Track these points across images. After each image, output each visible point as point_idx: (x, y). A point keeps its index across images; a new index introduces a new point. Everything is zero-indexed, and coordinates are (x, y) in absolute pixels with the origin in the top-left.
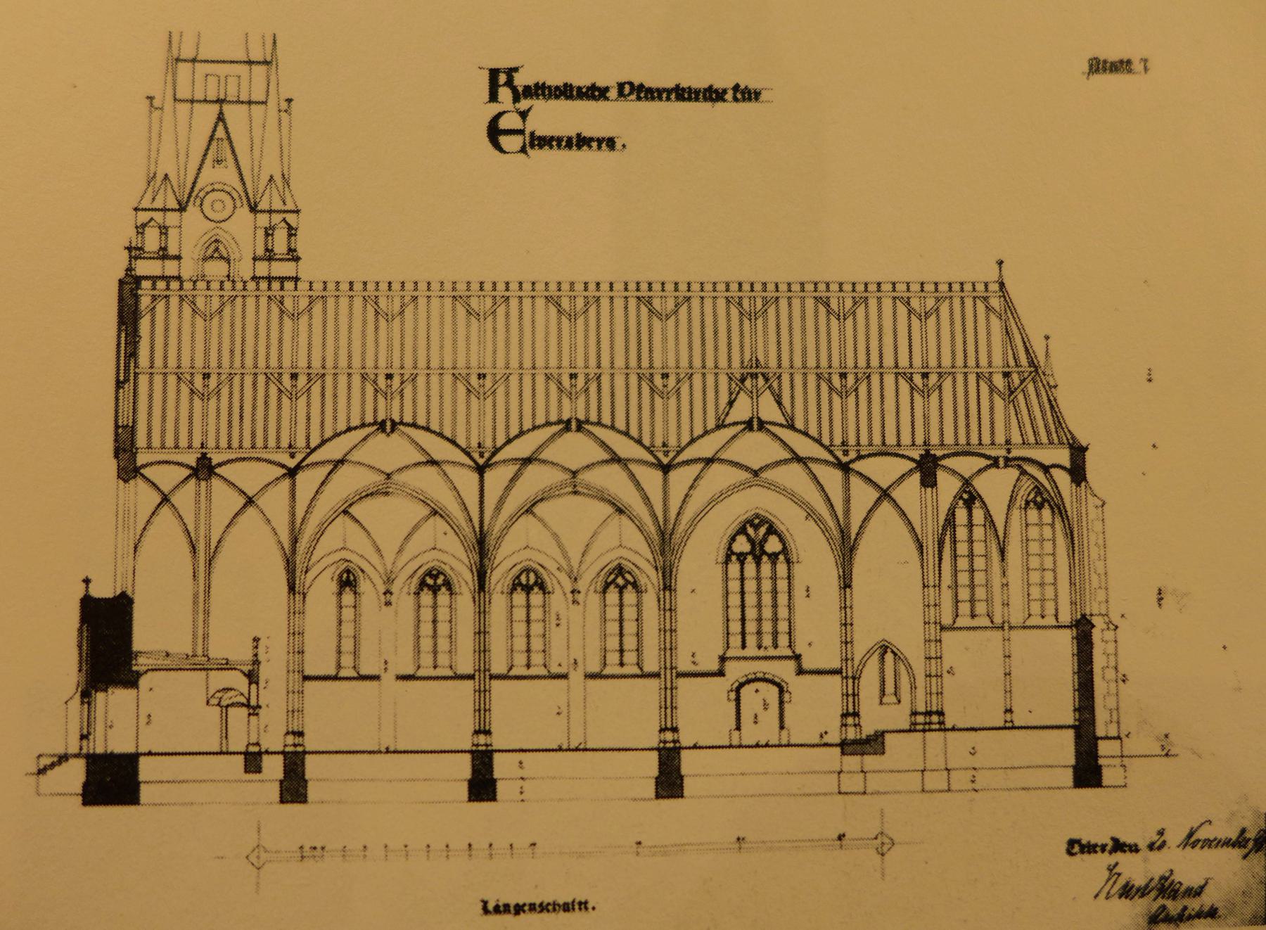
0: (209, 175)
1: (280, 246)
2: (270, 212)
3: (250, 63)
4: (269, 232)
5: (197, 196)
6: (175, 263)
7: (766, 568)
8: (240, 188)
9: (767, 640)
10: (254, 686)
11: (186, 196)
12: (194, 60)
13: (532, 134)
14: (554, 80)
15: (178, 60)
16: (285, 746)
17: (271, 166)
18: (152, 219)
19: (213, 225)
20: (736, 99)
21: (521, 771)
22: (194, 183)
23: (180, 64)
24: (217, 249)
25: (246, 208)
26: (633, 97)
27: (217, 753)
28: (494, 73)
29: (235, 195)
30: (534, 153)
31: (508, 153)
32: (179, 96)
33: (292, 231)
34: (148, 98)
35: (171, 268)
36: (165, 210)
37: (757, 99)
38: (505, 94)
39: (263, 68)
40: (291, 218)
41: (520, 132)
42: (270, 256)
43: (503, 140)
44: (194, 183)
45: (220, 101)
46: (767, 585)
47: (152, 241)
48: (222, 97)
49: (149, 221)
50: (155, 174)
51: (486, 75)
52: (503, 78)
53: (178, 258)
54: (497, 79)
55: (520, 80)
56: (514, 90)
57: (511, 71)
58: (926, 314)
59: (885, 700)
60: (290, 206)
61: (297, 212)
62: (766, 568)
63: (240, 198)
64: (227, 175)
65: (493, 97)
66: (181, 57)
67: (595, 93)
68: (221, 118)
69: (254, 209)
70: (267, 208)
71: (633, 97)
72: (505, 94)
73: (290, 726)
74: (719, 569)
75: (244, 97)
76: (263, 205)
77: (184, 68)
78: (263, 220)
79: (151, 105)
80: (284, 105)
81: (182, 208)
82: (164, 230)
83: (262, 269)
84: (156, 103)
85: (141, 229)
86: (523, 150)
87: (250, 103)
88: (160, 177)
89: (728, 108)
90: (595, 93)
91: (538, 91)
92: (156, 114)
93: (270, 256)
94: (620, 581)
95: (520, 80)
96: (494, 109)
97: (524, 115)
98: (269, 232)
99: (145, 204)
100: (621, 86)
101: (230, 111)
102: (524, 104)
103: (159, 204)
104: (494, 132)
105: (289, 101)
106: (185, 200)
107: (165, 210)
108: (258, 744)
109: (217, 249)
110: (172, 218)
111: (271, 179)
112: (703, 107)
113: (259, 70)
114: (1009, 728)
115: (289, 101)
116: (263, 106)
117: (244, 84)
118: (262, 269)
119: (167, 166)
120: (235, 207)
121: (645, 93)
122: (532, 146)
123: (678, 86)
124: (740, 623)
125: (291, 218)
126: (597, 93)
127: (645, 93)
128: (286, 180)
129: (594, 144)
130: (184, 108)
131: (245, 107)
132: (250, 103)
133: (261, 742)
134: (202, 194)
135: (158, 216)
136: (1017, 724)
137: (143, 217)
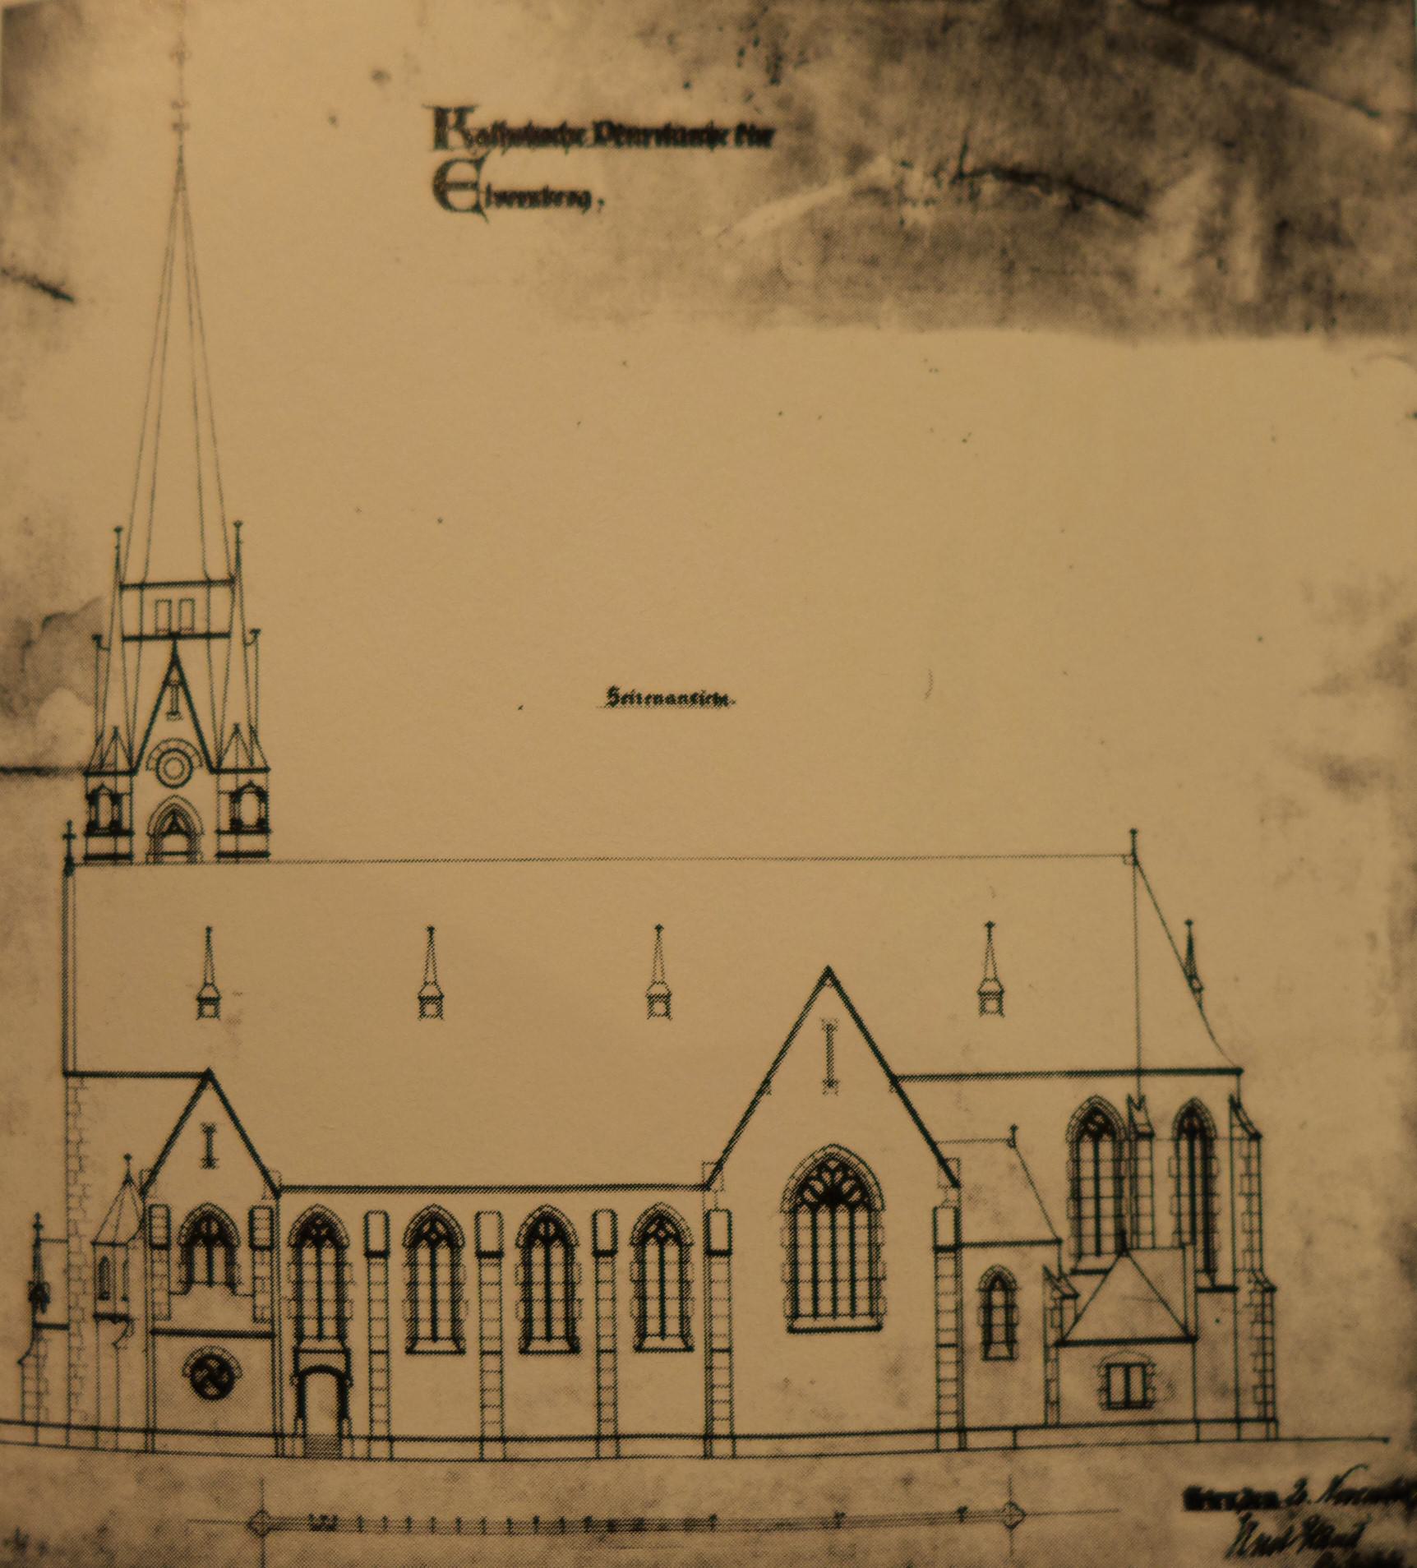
0: (164, 729)
3: (209, 583)
4: (236, 796)
5: (150, 757)
7: (843, 1218)
8: (194, 741)
9: (844, 1306)
10: (116, 808)
17: (236, 713)
18: (251, 784)
19: (169, 792)
24: (174, 823)
29: (190, 751)
30: (493, 212)
32: (257, 1243)
35: (123, 845)
38: (454, 138)
40: (258, 779)
42: (237, 827)
43: (454, 197)
46: (843, 1237)
48: (175, 628)
52: (452, 118)
55: (474, 122)
56: (466, 135)
57: (462, 112)
59: (994, 1352)
61: (266, 770)
62: (843, 1218)
63: (197, 753)
64: (183, 729)
65: (440, 141)
67: (563, 136)
68: (175, 662)
72: (454, 138)
74: (781, 1221)
75: (200, 628)
77: (131, 597)
78: (229, 782)
80: (250, 638)
81: (132, 772)
82: (116, 798)
83: (229, 843)
84: (105, 643)
86: (477, 208)
87: (208, 636)
91: (502, 135)
92: (103, 654)
93: (237, 827)
94: (662, 1234)
95: (474, 122)
96: (441, 156)
97: (478, 163)
100: (598, 126)
101: (186, 648)
104: (441, 188)
105: (256, 632)
109: (174, 823)
110: (122, 784)
115: (256, 632)
117: (200, 613)
118: (229, 843)
120: (192, 767)
124: (810, 1232)
125: (258, 779)
128: (253, 732)
130: (131, 647)
131: (202, 643)
132: (208, 636)
134: (156, 754)
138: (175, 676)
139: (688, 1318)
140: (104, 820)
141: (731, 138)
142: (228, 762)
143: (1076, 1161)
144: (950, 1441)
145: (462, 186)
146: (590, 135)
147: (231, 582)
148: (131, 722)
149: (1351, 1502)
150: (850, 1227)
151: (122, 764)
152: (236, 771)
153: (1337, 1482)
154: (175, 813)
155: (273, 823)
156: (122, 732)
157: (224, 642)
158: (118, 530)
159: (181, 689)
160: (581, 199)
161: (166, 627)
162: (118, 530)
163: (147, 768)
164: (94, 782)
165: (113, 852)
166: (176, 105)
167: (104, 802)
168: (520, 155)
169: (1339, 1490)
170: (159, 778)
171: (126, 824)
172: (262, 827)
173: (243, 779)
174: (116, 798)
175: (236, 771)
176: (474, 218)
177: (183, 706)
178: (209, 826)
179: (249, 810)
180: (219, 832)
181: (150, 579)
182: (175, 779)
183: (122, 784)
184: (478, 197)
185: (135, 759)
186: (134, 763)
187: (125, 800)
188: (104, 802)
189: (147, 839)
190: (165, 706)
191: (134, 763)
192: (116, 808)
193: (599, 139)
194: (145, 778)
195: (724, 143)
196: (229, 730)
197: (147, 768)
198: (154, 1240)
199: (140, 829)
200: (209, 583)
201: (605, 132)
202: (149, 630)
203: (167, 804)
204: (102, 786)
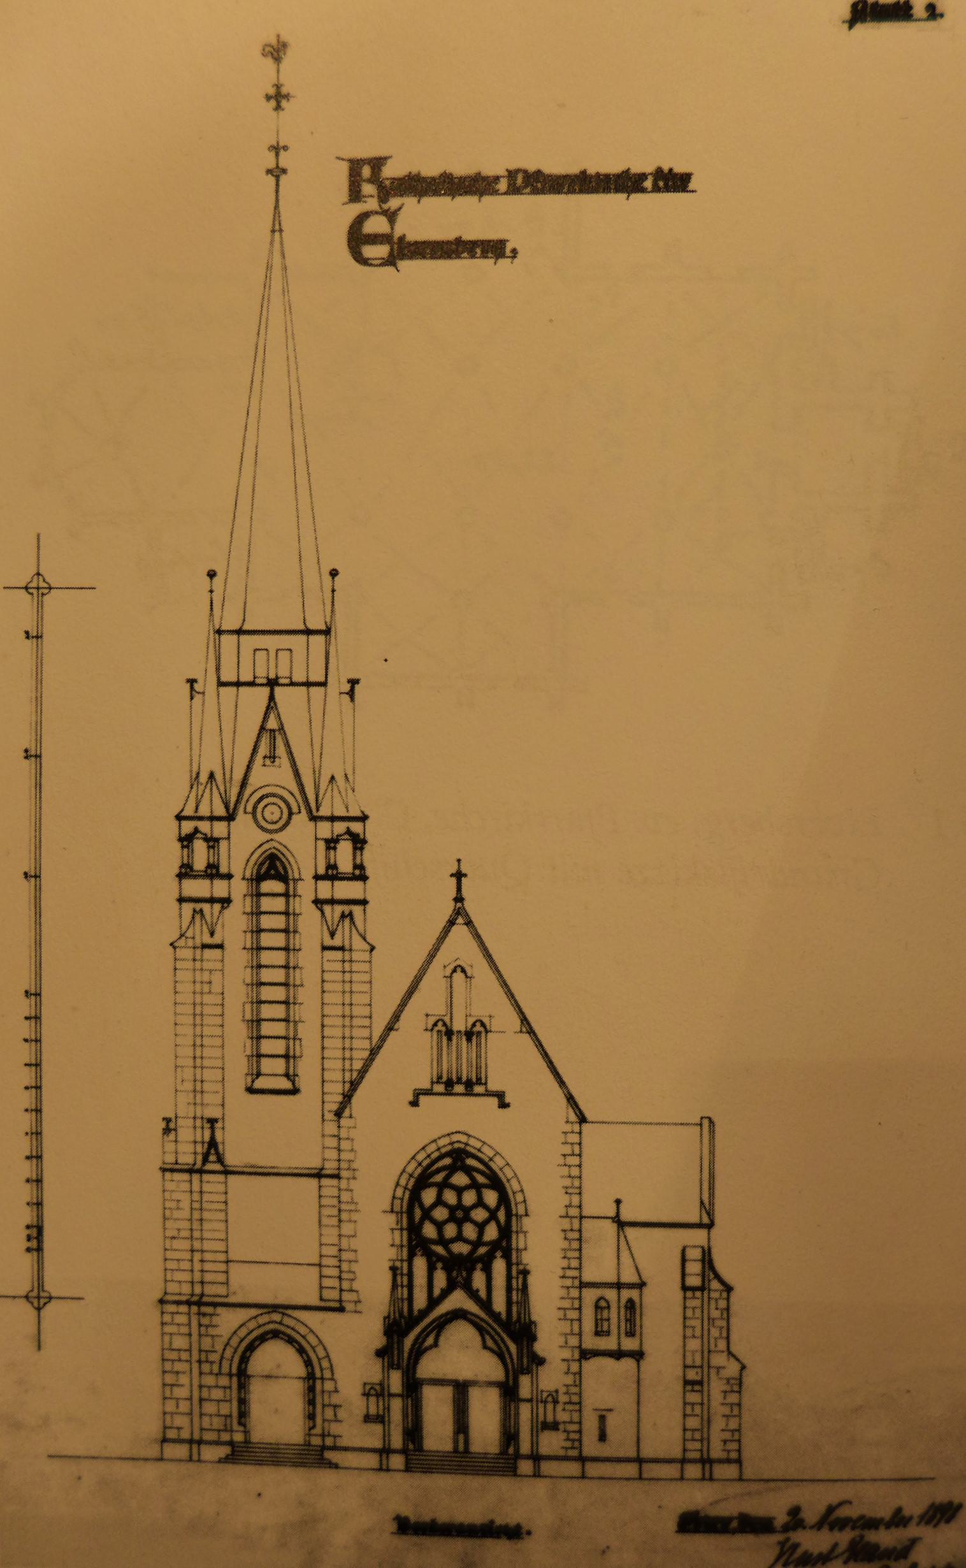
0: (261, 776)
1: (345, 866)
3: (308, 632)
4: (331, 843)
6: (225, 883)
12: (239, 632)
14: (430, 169)
15: (219, 632)
18: (196, 830)
19: (268, 836)
21: (600, 1445)
22: (244, 784)
23: (224, 637)
28: (355, 166)
33: (358, 842)
34: (414, 1103)
35: (220, 888)
36: (212, 818)
38: (368, 189)
39: (321, 639)
42: (332, 874)
44: (244, 784)
45: (272, 683)
47: (200, 856)
50: (198, 774)
51: (344, 167)
52: (366, 171)
53: (229, 876)
55: (390, 171)
57: (377, 163)
65: (355, 195)
66: (223, 628)
69: (314, 818)
72: (368, 189)
75: (299, 677)
79: (192, 688)
81: (230, 817)
82: (212, 842)
83: (325, 890)
88: (204, 778)
97: (391, 216)
98: (331, 843)
99: (189, 812)
100: (512, 174)
102: (393, 203)
103: (204, 811)
104: (357, 239)
107: (212, 818)
110: (220, 829)
111: (212, 776)
112: (616, 200)
113: (318, 641)
116: (322, 689)
118: (325, 890)
119: (210, 763)
120: (291, 814)
123: (584, 172)
125: (356, 827)
135: (204, 826)
137: (188, 827)
139: (618, 1359)
140: (200, 864)
142: (324, 811)
143: (41, 1150)
144: (693, 1471)
145: (374, 239)
146: (503, 185)
147: (327, 632)
148: (317, 766)
149: (837, 1528)
150: (685, 1275)
151: (220, 811)
152: (333, 819)
153: (831, 1509)
156: (219, 776)
157: (321, 689)
158: (212, 575)
160: (495, 249)
161: (264, 675)
162: (212, 575)
163: (245, 812)
165: (330, 898)
166: (277, 149)
167: (199, 846)
168: (435, 204)
169: (833, 1517)
171: (223, 869)
172: (360, 874)
173: (340, 827)
174: (212, 842)
175: (333, 819)
176: (390, 269)
177: (281, 750)
178: (308, 874)
180: (317, 877)
181: (246, 627)
183: (220, 829)
184: (392, 249)
185: (232, 806)
186: (231, 811)
188: (199, 846)
190: (263, 750)
191: (231, 811)
193: (513, 190)
194: (243, 820)
197: (245, 812)
198: (35, 1247)
199: (237, 871)
200: (308, 632)
202: (246, 677)
203: (267, 853)
204: (196, 830)
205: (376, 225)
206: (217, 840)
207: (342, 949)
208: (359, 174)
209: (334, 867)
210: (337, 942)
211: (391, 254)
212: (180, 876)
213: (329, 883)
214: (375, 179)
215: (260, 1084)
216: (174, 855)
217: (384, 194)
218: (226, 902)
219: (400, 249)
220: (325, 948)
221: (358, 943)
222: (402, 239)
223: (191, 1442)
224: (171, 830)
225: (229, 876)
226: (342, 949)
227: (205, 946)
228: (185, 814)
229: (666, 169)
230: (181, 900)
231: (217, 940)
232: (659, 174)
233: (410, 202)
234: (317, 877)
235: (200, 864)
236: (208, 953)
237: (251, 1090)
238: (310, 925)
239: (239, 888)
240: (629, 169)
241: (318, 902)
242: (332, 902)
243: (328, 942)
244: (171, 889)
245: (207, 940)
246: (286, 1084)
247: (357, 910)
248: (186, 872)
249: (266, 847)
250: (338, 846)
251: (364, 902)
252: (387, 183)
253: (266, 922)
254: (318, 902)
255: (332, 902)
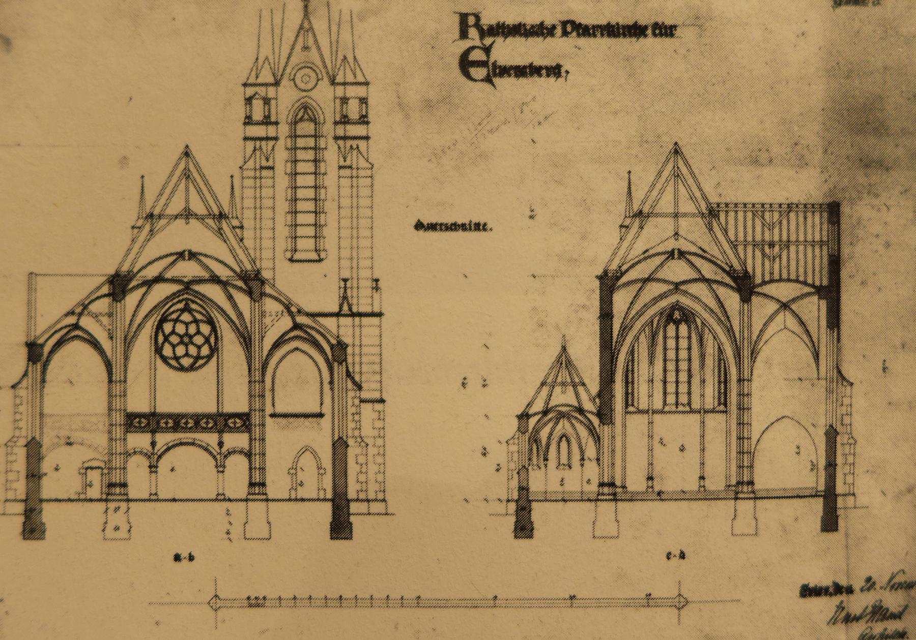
2: (344, 84)
4: (344, 100)
11: (281, 70)
13: (494, 64)
16: (151, 494)
18: (256, 93)
20: (655, 35)
25: (326, 81)
26: (574, 34)
27: (212, 500)
31: (475, 80)
35: (271, 131)
37: (672, 35)
38: (473, 33)
40: (361, 91)
41: (483, 64)
42: (345, 120)
49: (255, 95)
51: (457, 19)
52: (471, 20)
53: (277, 123)
54: (463, 23)
55: (487, 20)
58: (773, 224)
60: (360, 79)
65: (464, 35)
67: (541, 31)
69: (333, 82)
70: (342, 81)
71: (574, 34)
72: (473, 33)
73: (510, 496)
76: (339, 79)
78: (340, 91)
81: (277, 84)
82: (266, 101)
83: (340, 131)
85: (249, 100)
86: (488, 80)
89: (650, 42)
90: (541, 31)
93: (345, 120)
96: (466, 44)
97: (487, 50)
99: (252, 80)
100: (564, 24)
102: (488, 41)
104: (465, 64)
106: (280, 74)
108: (156, 494)
110: (271, 92)
114: (220, 500)
118: (340, 131)
120: (318, 80)
121: (584, 31)
122: (495, 75)
126: (545, 31)
127: (584, 31)
129: (544, 72)
133: (158, 493)
135: (262, 91)
136: (161, 496)
137: (250, 91)
138: (306, 25)
140: (258, 116)
141: (649, 32)
146: (559, 31)
151: (271, 80)
154: (305, 107)
155: (371, 117)
159: (310, 35)
160: (555, 71)
164: (250, 91)
167: (258, 104)
170: (296, 86)
171: (273, 119)
176: (486, 86)
179: (353, 110)
180: (336, 123)
182: (297, 349)
184: (489, 71)
187: (273, 102)
189: (287, 178)
192: (267, 107)
195: (646, 36)
196: (340, 57)
199: (282, 118)
201: (569, 28)
205: (477, 55)
206: (269, 100)
207: (350, 167)
208: (467, 22)
209: (346, 116)
210: (348, 163)
211: (488, 75)
212: (245, 124)
213: (343, 126)
214: (477, 25)
215: (298, 256)
216: (240, 112)
217: (483, 34)
218: (276, 139)
219: (494, 70)
220: (340, 167)
221: (363, 163)
222: (494, 64)
223: (203, 220)
224: (240, 94)
225: (277, 123)
226: (350, 167)
227: (262, 168)
228: (249, 82)
229: (660, 23)
230: (246, 139)
231: (270, 164)
232: (656, 26)
233: (499, 40)
234: (336, 123)
235: (258, 116)
236: (265, 173)
237: (291, 260)
238: (331, 156)
239: (284, 130)
240: (636, 22)
241: (336, 138)
242: (345, 138)
243: (342, 163)
244: (239, 130)
245: (264, 163)
246: (314, 256)
247: (362, 144)
248: (248, 121)
249: (302, 101)
250: (349, 102)
251: (367, 138)
252: (485, 28)
253: (310, 193)
254: (336, 138)
255: (345, 138)
